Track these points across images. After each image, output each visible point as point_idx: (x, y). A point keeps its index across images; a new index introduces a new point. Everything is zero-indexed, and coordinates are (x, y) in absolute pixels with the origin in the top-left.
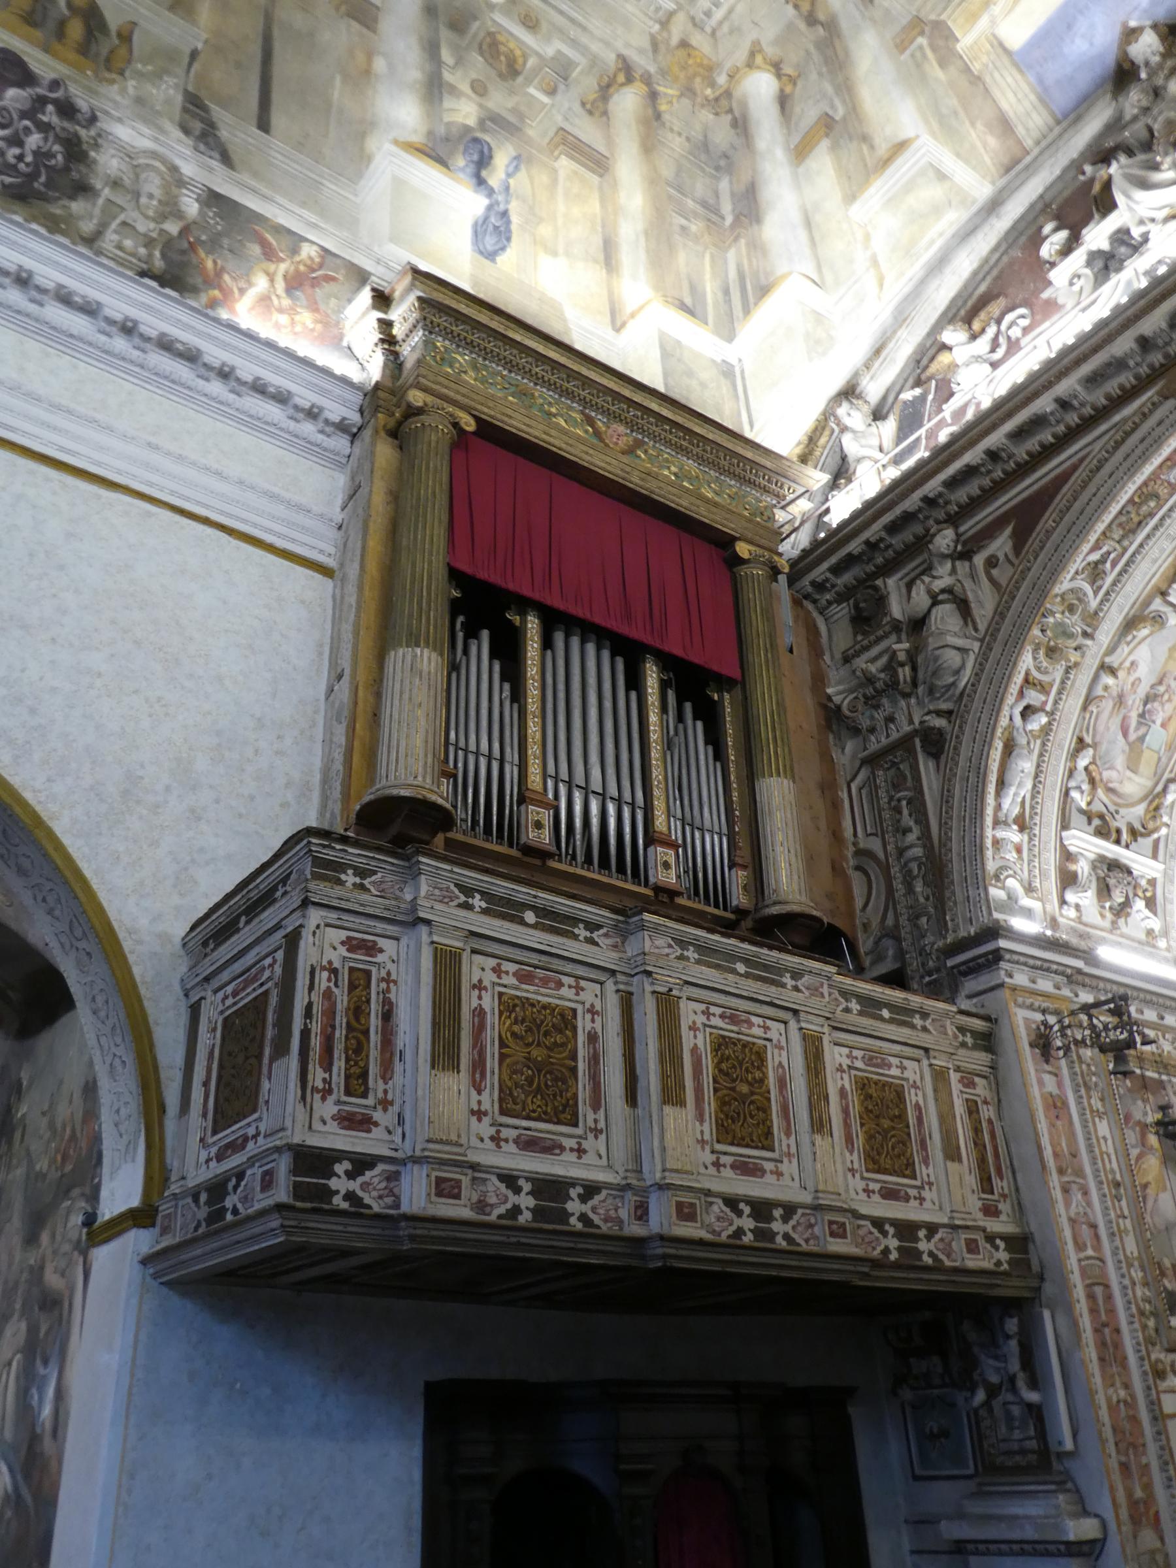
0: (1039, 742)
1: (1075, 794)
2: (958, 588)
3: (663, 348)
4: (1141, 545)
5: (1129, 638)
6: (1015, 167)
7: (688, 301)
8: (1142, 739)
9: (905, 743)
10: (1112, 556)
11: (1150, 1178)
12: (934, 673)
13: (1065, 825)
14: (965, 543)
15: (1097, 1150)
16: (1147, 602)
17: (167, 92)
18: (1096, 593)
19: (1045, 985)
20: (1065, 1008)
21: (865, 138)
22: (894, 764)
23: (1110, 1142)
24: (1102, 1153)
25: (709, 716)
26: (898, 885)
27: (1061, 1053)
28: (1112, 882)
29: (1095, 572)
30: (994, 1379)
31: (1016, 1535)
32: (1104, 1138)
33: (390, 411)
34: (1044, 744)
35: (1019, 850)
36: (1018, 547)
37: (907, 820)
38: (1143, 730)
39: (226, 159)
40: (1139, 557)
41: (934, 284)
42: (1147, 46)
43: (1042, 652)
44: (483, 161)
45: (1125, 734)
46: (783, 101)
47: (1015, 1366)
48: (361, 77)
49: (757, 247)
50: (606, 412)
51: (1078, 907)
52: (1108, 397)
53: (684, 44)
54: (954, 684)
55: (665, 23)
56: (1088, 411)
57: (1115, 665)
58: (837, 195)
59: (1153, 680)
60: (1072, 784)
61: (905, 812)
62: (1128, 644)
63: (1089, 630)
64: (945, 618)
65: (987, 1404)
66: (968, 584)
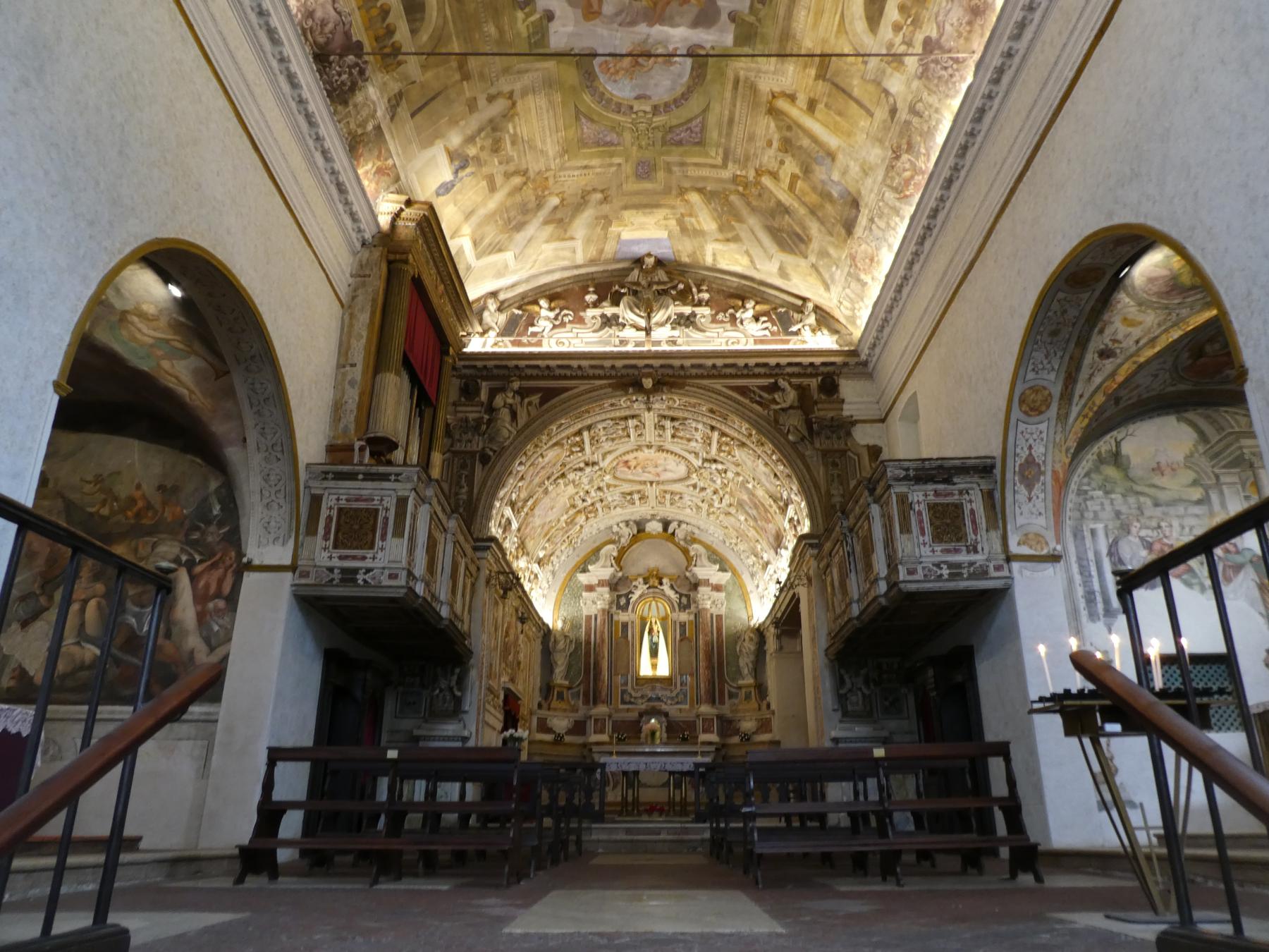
6: (592, 262)
9: (473, 454)
17: (395, 87)
25: (421, 415)
33: (387, 241)
39: (392, 118)
42: (650, 261)
44: (463, 167)
46: (556, 208)
47: (453, 683)
48: (454, 122)
49: (510, 239)
53: (547, 179)
55: (547, 170)
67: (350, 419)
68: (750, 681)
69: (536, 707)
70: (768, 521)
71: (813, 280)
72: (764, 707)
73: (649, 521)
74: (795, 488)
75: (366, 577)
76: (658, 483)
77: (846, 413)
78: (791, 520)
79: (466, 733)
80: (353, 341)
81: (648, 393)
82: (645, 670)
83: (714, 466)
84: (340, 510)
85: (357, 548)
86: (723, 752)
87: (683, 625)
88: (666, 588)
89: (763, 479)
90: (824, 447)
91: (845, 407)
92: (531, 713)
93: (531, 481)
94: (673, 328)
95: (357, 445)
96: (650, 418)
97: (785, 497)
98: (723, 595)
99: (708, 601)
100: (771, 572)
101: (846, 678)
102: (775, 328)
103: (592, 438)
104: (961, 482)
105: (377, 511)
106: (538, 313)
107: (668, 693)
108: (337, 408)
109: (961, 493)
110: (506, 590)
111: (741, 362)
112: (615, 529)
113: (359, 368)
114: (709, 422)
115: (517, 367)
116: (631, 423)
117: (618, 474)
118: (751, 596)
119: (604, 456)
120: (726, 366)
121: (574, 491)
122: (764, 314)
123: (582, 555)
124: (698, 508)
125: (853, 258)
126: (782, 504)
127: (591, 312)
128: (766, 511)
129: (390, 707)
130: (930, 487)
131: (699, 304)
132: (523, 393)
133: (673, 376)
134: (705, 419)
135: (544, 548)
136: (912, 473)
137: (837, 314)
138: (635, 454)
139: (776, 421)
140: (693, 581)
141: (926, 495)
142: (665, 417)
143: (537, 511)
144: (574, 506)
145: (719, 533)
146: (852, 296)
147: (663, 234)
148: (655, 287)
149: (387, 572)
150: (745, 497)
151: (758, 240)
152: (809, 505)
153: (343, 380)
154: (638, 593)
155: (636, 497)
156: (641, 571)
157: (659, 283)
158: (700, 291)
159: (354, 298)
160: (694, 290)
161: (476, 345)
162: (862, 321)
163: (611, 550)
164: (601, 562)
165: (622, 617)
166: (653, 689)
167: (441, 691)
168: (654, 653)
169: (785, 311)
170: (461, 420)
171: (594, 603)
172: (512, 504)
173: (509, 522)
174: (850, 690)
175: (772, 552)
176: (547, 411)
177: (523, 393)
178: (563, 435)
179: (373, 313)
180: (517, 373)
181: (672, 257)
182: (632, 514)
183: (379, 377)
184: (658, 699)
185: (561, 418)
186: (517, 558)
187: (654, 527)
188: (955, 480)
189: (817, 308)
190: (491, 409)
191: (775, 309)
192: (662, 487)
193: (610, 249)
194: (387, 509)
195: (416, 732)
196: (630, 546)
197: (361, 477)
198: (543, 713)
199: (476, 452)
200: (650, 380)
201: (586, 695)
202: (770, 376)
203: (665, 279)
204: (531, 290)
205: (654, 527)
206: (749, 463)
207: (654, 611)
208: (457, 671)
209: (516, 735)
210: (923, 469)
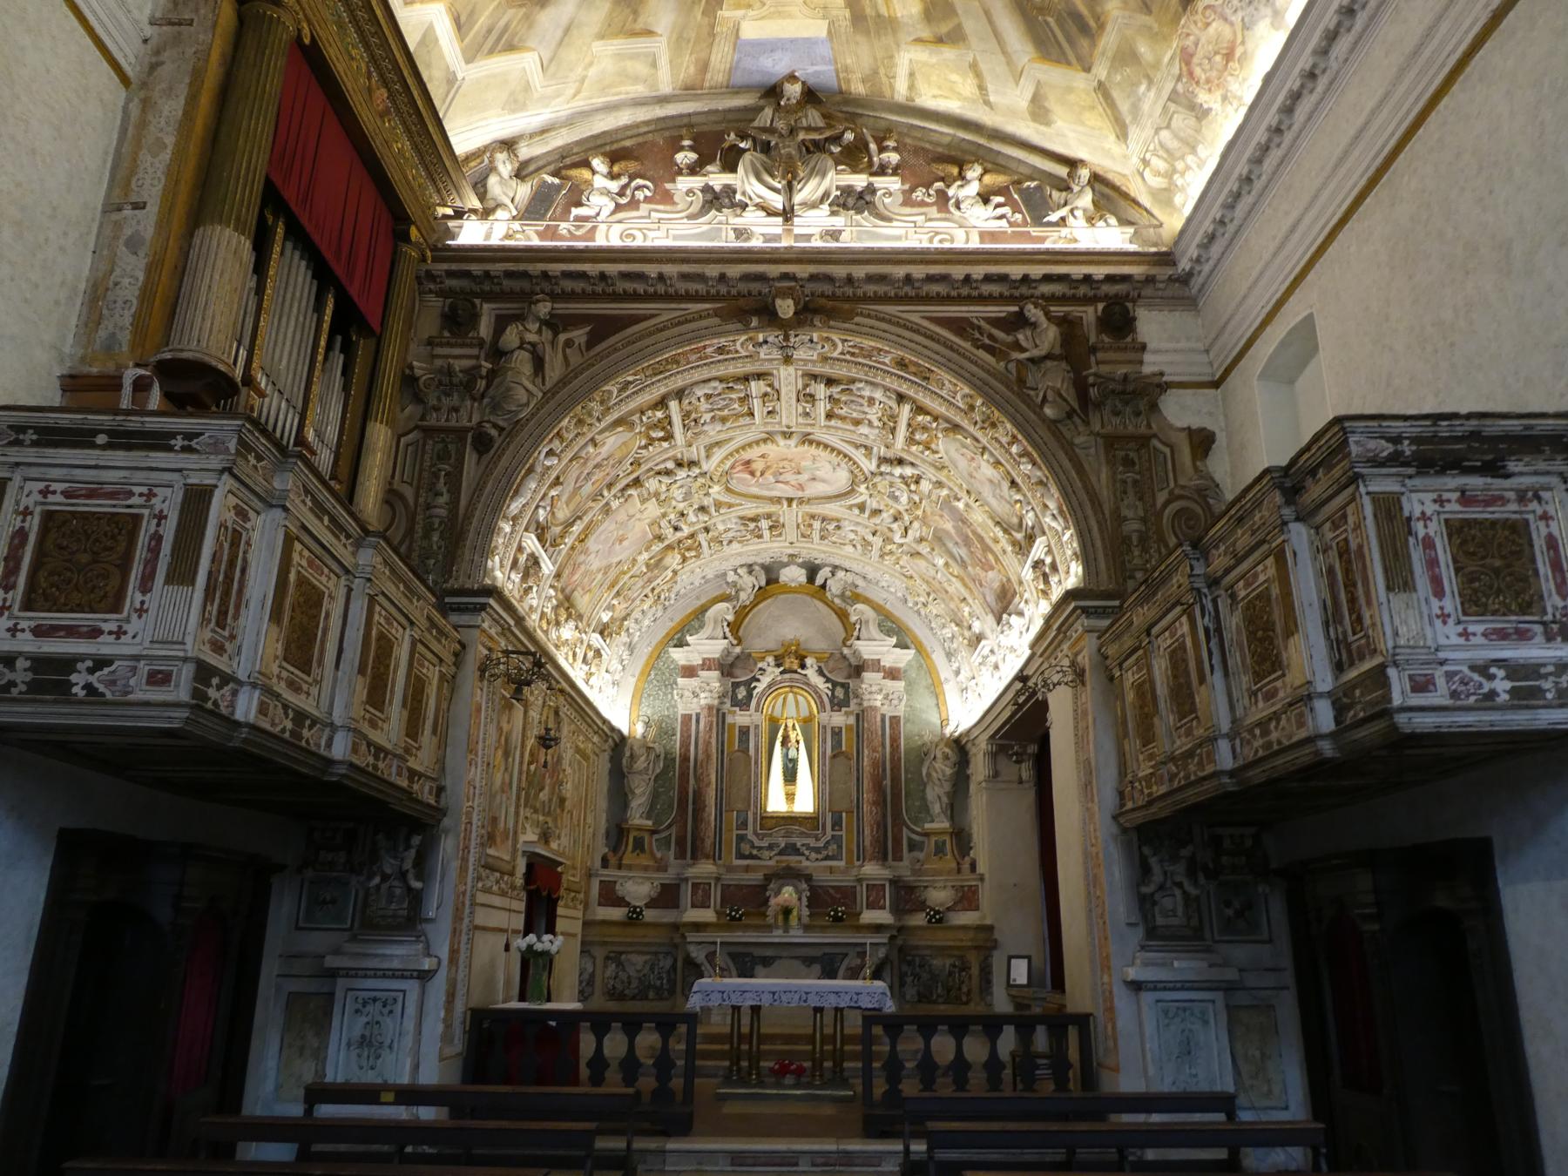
1: (541, 511)
3: (424, 36)
6: (689, 90)
7: (463, 19)
9: (461, 433)
21: (635, 13)
22: (443, 441)
25: (348, 349)
26: (419, 529)
30: (388, 871)
31: (386, 965)
36: (590, 344)
37: (441, 485)
41: (600, 116)
42: (793, 91)
47: (408, 865)
49: (529, 20)
50: (381, 75)
52: (687, 292)
56: (671, 291)
58: (595, 29)
61: (442, 480)
65: (378, 887)
66: (548, 348)
67: (121, 321)
68: (944, 824)
69: (598, 863)
70: (987, 567)
71: (1097, 120)
72: (966, 866)
73: (786, 565)
74: (1052, 505)
75: (93, 679)
76: (801, 501)
77: (1147, 369)
78: (1038, 564)
79: (427, 964)
80: (145, 158)
81: (785, 326)
83: (898, 471)
84: (48, 516)
85: (79, 608)
86: (899, 942)
87: (836, 733)
88: (811, 673)
89: (987, 492)
90: (1109, 429)
91: (1147, 357)
92: (589, 875)
93: (577, 489)
94: (833, 213)
95: (130, 375)
96: (788, 379)
97: (1029, 519)
98: (901, 685)
99: (877, 694)
100: (986, 651)
101: (1153, 861)
102: (1018, 216)
103: (686, 415)
104: (1524, 472)
105: (137, 519)
106: (589, 183)
107: (812, 842)
108: (97, 295)
109: (1522, 497)
110: (519, 684)
111: (958, 272)
112: (731, 577)
113: (153, 209)
114: (895, 386)
115: (545, 274)
116: (756, 387)
117: (734, 485)
118: (947, 687)
119: (709, 449)
120: (930, 279)
121: (659, 512)
122: (998, 193)
123: (678, 619)
124: (867, 544)
125: (1186, 57)
126: (1019, 536)
127: (684, 183)
128: (986, 548)
129: (282, 910)
130: (1453, 481)
131: (882, 171)
132: (555, 324)
133: (833, 297)
134: (888, 382)
135: (611, 607)
136: (1407, 448)
137: (1136, 189)
138: (763, 449)
139: (1021, 381)
140: (854, 662)
141: (1440, 501)
142: (815, 377)
143: (591, 543)
144: (660, 538)
145: (898, 586)
146: (1173, 144)
147: (816, 29)
148: (802, 136)
149: (144, 668)
150: (949, 526)
151: (997, 35)
152: (1083, 535)
153: (116, 238)
154: (765, 681)
155: (764, 524)
156: (772, 645)
157: (809, 129)
158: (882, 149)
159: (153, 67)
160: (873, 146)
161: (471, 234)
162: (1186, 202)
163: (724, 611)
164: (707, 631)
165: (740, 718)
166: (788, 835)
167: (385, 878)
168: (790, 776)
169: (1038, 184)
170: (440, 371)
171: (696, 696)
172: (541, 532)
173: (535, 561)
174: (1161, 887)
175: (990, 619)
176: (601, 357)
177: (555, 324)
178: (632, 405)
179: (192, 99)
180: (547, 287)
181: (833, 83)
182: (758, 553)
183: (199, 232)
185: (625, 369)
186: (558, 624)
187: (794, 575)
188: (1513, 466)
189: (1097, 179)
190: (498, 354)
191: (1019, 182)
192: (807, 508)
193: (721, 59)
194: (161, 517)
195: (331, 962)
196: (754, 604)
197: (101, 439)
198: (610, 874)
199: (466, 430)
200: (790, 302)
201: (681, 842)
202: (1011, 299)
203: (821, 124)
204: (577, 143)
205: (794, 575)
206: (962, 463)
207: (791, 710)
208: (416, 840)
209: (539, 947)
210: (1434, 439)
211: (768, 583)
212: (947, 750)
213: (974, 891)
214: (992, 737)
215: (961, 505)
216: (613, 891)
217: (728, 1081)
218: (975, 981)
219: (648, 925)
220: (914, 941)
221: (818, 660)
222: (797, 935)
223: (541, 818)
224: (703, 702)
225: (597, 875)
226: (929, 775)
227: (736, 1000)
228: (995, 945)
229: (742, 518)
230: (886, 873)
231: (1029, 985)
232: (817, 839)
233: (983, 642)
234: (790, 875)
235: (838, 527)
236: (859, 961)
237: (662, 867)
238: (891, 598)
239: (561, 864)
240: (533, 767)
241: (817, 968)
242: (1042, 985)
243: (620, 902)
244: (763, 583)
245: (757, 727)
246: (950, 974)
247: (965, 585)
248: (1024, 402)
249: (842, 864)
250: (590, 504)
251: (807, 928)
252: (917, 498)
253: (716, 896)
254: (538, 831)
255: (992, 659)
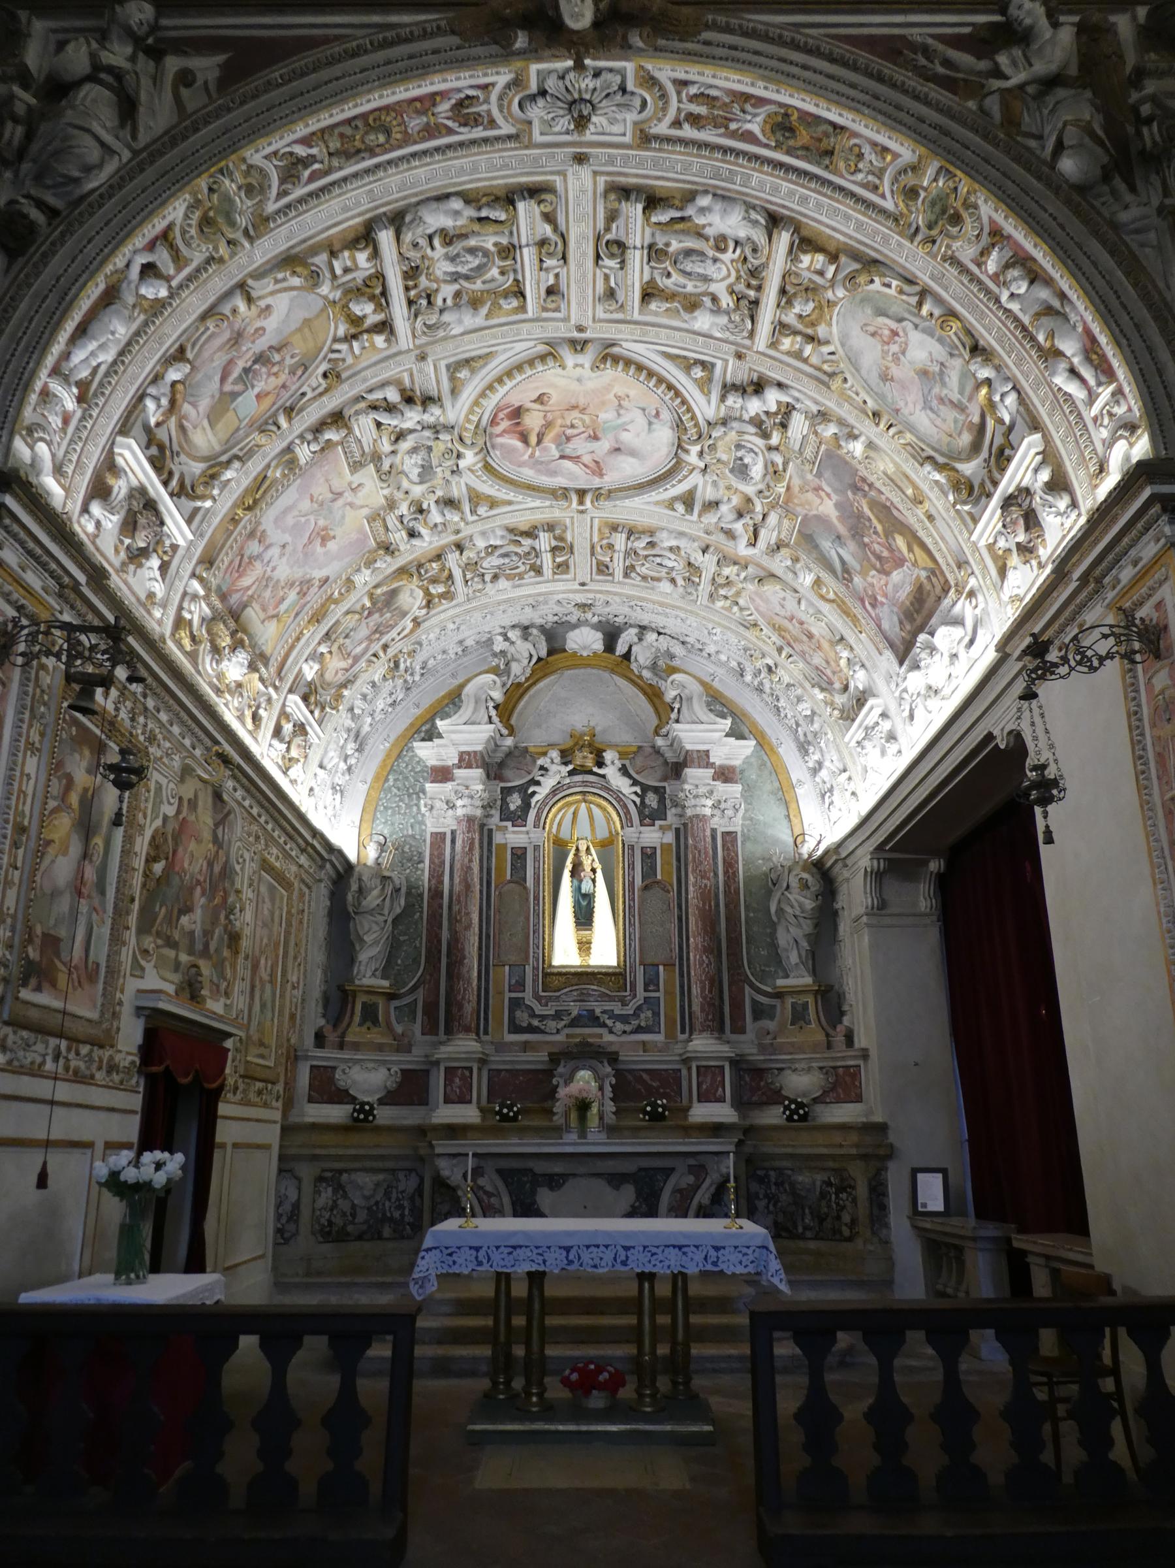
0: (142, 317)
1: (150, 405)
2: (129, 79)
4: (345, 179)
5: (280, 276)
8: (234, 395)
10: (316, 166)
11: (55, 836)
12: (56, 153)
13: (124, 429)
14: (157, 40)
15: (16, 785)
16: (314, 251)
18: (282, 194)
19: (33, 579)
20: (44, 615)
23: (32, 782)
24: (20, 791)
27: (20, 660)
28: (142, 521)
29: (292, 168)
32: (28, 775)
34: (146, 324)
35: (66, 421)
38: (239, 388)
40: (337, 191)
43: (197, 215)
45: (223, 379)
51: (98, 524)
54: (77, 181)
57: (254, 294)
59: (274, 343)
60: (152, 390)
62: (277, 281)
63: (252, 233)
64: (95, 106)
66: (145, 82)
69: (309, 1040)
72: (839, 1039)
73: (575, 626)
76: (598, 494)
81: (578, 46)
82: (565, 952)
87: (649, 855)
88: (611, 772)
92: (294, 1057)
96: (580, 190)
99: (701, 794)
100: (874, 716)
107: (618, 1009)
112: (499, 645)
118: (800, 791)
139: (1011, 122)
144: (388, 549)
150: (828, 508)
154: (548, 783)
156: (556, 738)
165: (513, 837)
166: (583, 998)
168: (584, 917)
172: (160, 458)
175: (888, 659)
184: (593, 1020)
198: (327, 1056)
201: (430, 1010)
211: (550, 653)
212: (805, 875)
213: (853, 1074)
214: (880, 848)
215: (857, 448)
216: (332, 1080)
217: (488, 1406)
218: (863, 1210)
219: (379, 1129)
220: (768, 1148)
221: (622, 755)
222: (597, 1141)
223: (184, 958)
224: (460, 812)
225: (307, 1058)
226: (780, 911)
227: (500, 1263)
228: (890, 1153)
229: (511, 531)
230: (725, 1050)
231: (947, 1213)
232: (624, 1004)
233: (871, 702)
234: (588, 1054)
235: (652, 544)
236: (691, 1179)
237: (403, 1045)
238: (721, 672)
239: (229, 1035)
240: (158, 868)
241: (628, 1193)
242: (964, 1214)
243: (341, 1096)
244: (543, 653)
245: (537, 848)
246: (823, 1195)
247: (846, 612)
248: (1017, 159)
249: (660, 1038)
250: (261, 439)
251: (612, 1131)
252: (778, 459)
253: (480, 1085)
254: (177, 978)
255: (886, 726)
